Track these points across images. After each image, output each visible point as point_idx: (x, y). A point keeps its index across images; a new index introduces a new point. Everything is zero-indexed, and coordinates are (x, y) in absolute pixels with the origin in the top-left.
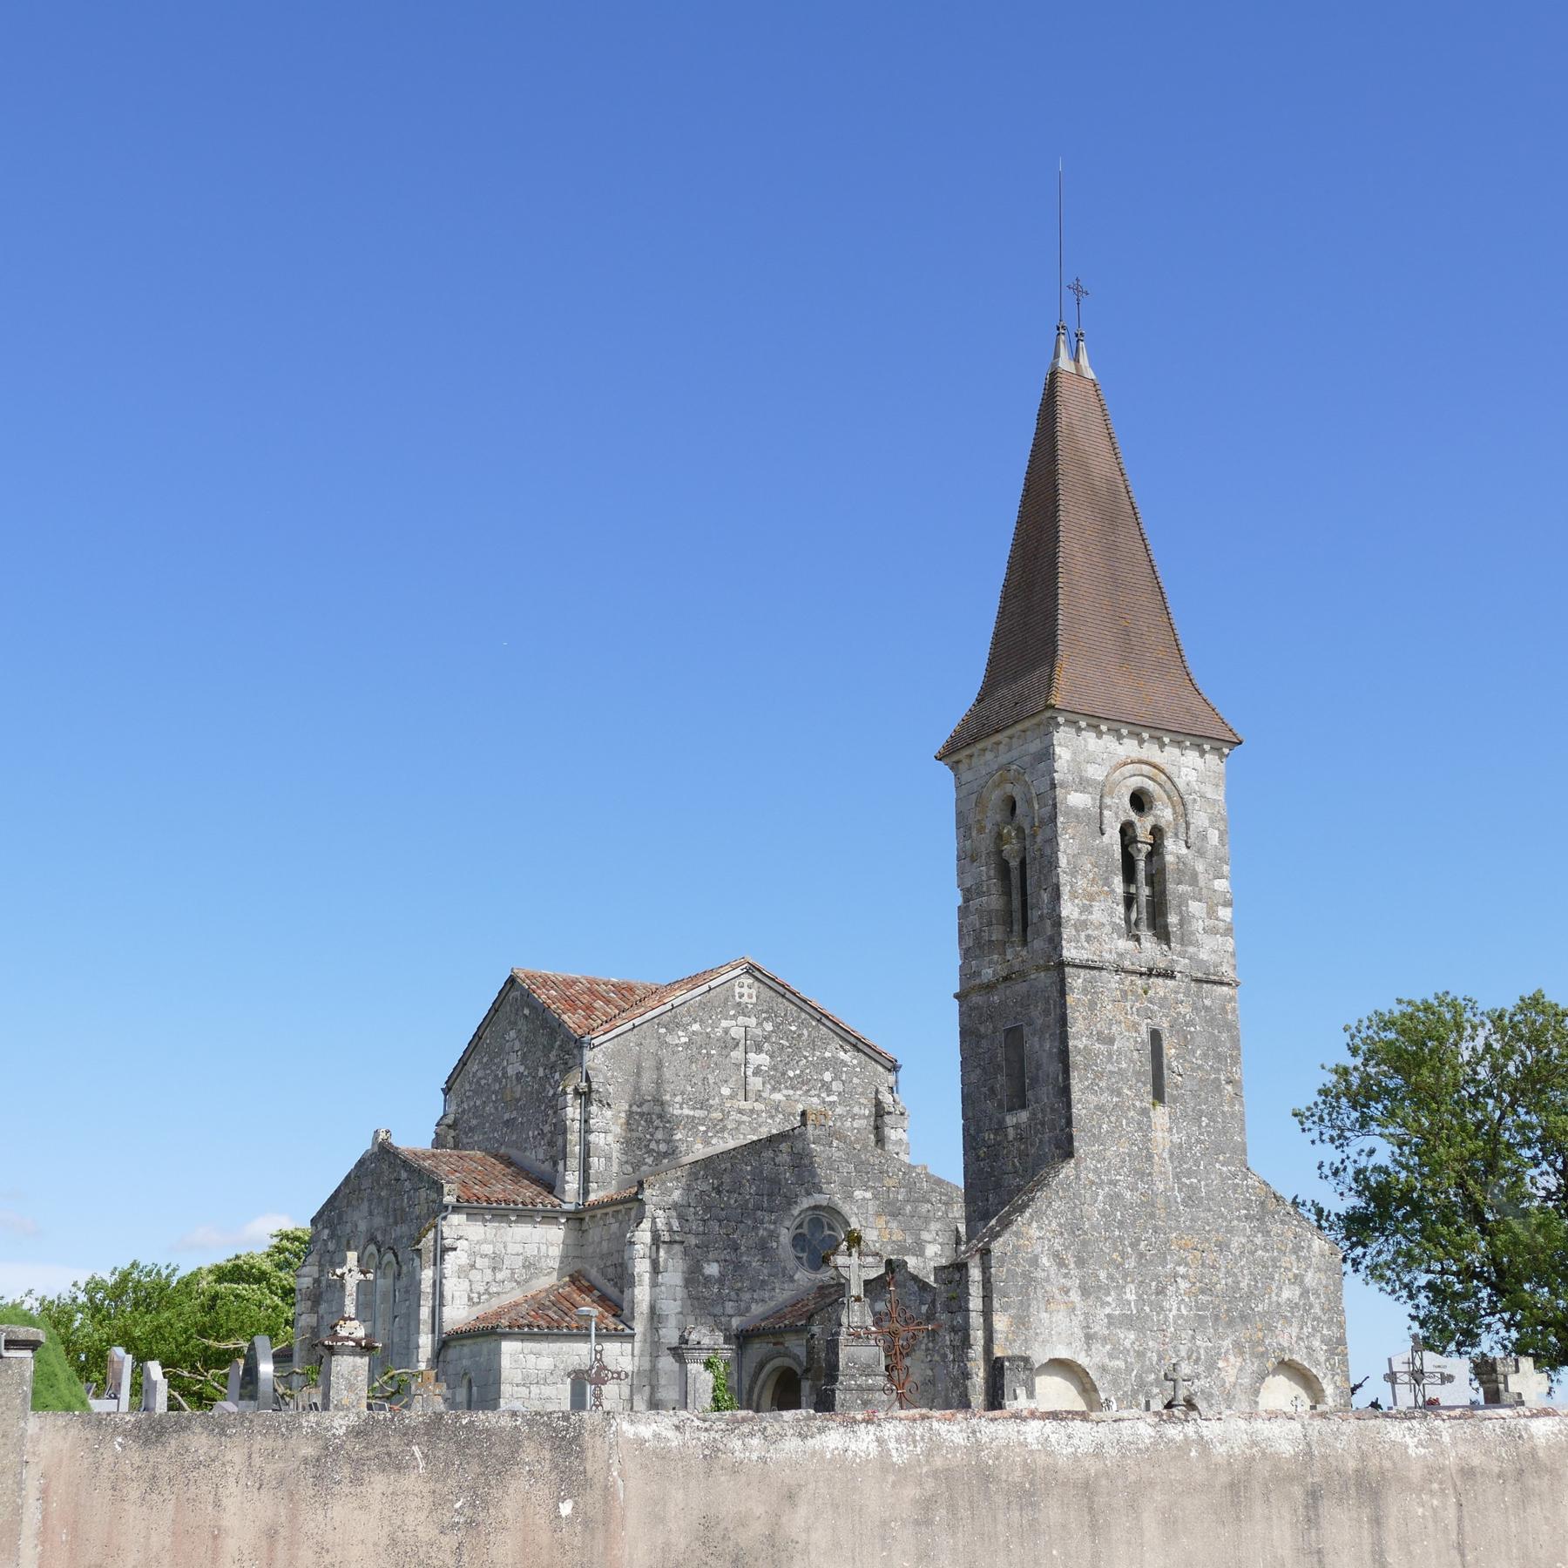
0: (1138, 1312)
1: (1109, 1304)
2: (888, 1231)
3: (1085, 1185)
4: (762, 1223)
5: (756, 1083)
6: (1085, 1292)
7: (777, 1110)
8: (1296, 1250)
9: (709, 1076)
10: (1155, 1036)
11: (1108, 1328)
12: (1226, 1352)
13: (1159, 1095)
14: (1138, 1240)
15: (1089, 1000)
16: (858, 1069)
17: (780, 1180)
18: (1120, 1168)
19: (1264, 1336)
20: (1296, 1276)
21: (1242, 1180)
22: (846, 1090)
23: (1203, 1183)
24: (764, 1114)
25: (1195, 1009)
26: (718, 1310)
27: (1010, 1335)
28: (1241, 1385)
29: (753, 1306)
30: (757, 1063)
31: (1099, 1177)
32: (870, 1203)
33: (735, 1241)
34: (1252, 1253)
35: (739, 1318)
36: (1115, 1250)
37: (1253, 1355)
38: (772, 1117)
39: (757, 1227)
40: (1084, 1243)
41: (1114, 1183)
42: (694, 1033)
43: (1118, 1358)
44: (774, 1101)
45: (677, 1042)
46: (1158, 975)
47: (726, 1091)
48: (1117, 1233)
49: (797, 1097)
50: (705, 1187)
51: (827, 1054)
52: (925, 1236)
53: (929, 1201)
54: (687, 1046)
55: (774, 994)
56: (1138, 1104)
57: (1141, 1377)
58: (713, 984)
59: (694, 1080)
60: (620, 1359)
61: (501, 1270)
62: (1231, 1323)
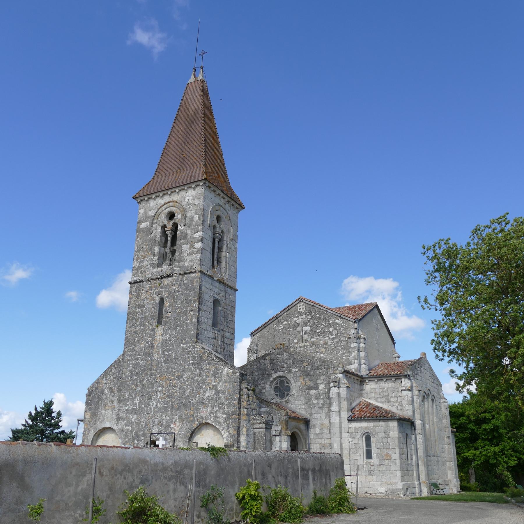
0: (139, 407)
1: (128, 405)
3: (126, 361)
4: (260, 384)
5: (305, 337)
6: (119, 401)
7: (313, 344)
8: (214, 375)
10: (162, 300)
11: (126, 414)
12: (176, 421)
13: (159, 323)
14: (143, 380)
15: (137, 294)
16: (343, 325)
18: (140, 353)
19: (194, 413)
20: (213, 386)
21: (192, 349)
22: (338, 333)
23: (174, 353)
24: (308, 347)
25: (180, 286)
27: (90, 420)
28: (180, 434)
30: (306, 330)
31: (131, 357)
32: (298, 372)
34: (193, 378)
36: (133, 384)
37: (188, 421)
38: (311, 347)
40: (122, 383)
41: (137, 359)
42: (285, 324)
43: (129, 426)
44: (312, 341)
46: (165, 277)
47: (295, 341)
48: (135, 378)
49: (320, 339)
51: (331, 322)
52: (319, 382)
56: (151, 327)
57: (137, 433)
62: (178, 409)
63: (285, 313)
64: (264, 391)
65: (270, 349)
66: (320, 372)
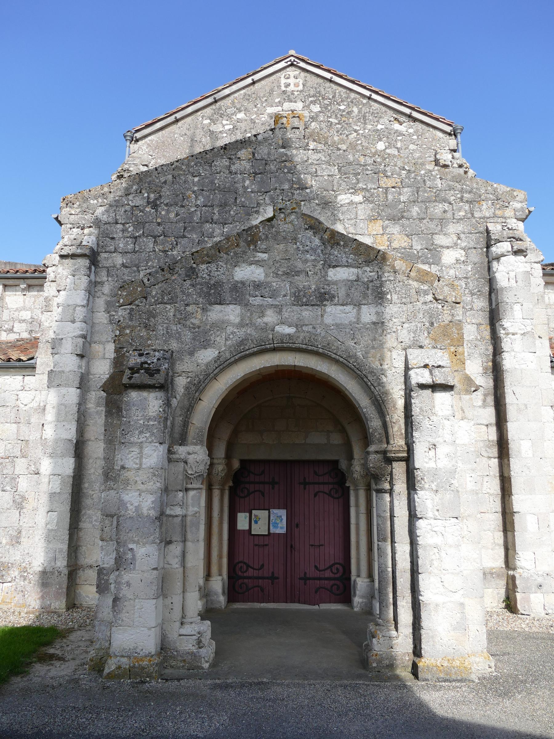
2: (385, 237)
16: (415, 137)
17: (237, 188)
32: (360, 207)
39: (204, 241)
42: (239, 121)
45: (221, 129)
50: (138, 201)
51: (380, 127)
53: (445, 200)
55: (321, 81)
63: (242, 92)
66: (445, 212)
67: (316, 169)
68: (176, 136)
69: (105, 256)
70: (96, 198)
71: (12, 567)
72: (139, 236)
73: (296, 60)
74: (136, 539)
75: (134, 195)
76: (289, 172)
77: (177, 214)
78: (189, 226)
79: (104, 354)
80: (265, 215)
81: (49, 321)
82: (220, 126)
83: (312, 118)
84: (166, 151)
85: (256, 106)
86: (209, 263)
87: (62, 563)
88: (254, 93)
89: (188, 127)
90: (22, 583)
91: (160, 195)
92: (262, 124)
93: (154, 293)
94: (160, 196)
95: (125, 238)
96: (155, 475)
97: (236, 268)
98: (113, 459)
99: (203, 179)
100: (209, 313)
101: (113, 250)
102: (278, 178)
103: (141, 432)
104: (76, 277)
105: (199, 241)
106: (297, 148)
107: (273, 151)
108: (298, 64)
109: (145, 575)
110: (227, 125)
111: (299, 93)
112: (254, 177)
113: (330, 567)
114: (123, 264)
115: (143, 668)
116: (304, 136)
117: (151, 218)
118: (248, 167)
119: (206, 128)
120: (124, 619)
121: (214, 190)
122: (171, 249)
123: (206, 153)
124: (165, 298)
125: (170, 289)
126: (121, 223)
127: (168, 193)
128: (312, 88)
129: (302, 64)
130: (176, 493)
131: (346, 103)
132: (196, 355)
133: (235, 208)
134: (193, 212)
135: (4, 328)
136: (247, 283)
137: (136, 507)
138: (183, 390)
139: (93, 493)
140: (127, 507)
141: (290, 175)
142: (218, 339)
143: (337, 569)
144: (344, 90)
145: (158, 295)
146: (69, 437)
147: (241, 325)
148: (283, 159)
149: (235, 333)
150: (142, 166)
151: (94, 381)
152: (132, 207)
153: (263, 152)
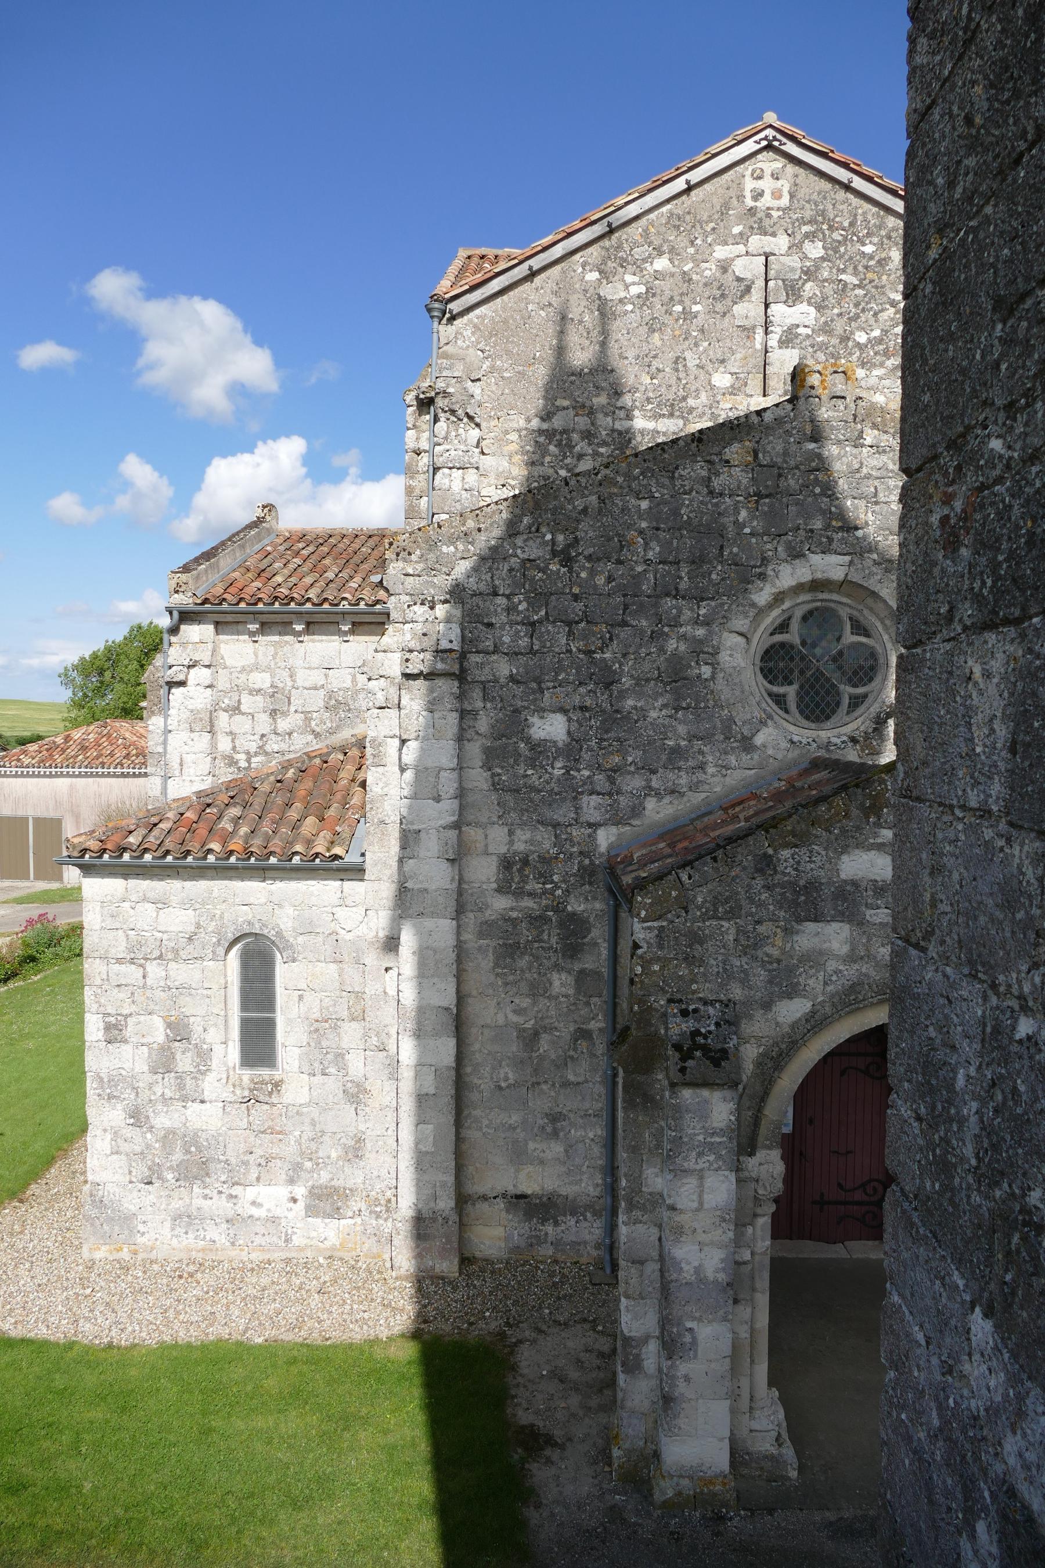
4: (676, 623)
9: (688, 355)
17: (724, 527)
26: (563, 813)
29: (651, 804)
30: (789, 321)
33: (605, 666)
35: (614, 830)
39: (663, 633)
42: (658, 275)
45: (623, 294)
47: (722, 380)
49: (873, 381)
50: (534, 551)
54: (644, 300)
55: (827, 186)
58: (695, 176)
59: (656, 364)
60: (340, 913)
61: (285, 714)
63: (664, 209)
64: (706, 671)
65: (560, 409)
67: (876, 488)
68: (530, 307)
69: (478, 660)
70: (452, 541)
71: (353, 1195)
72: (540, 622)
73: (779, 136)
74: (697, 1315)
75: (525, 537)
76: (823, 494)
77: (609, 577)
78: (634, 604)
79: (486, 846)
80: (777, 581)
81: (381, 785)
82: (620, 286)
83: (807, 272)
84: (512, 342)
85: (692, 243)
86: (796, 846)
87: (446, 1203)
88: (689, 213)
89: (555, 288)
90: (374, 1222)
91: (576, 538)
92: (706, 285)
93: (700, 899)
94: (576, 540)
95: (512, 624)
96: (725, 1221)
97: (843, 857)
98: (640, 1176)
99: (658, 504)
100: (795, 938)
101: (491, 648)
102: (802, 505)
103: (700, 1155)
104: (437, 715)
105: (653, 632)
106: (839, 442)
107: (794, 448)
108: (782, 147)
109: (713, 1365)
110: (634, 284)
111: (781, 213)
112: (757, 502)
113: (863, 1185)
114: (511, 676)
115: (715, 1495)
116: (855, 416)
117: (560, 585)
118: (745, 481)
119: (591, 290)
120: (682, 1426)
121: (679, 529)
122: (601, 649)
123: (663, 449)
124: (720, 910)
125: (727, 894)
126: (503, 595)
127: (591, 534)
128: (808, 202)
129: (791, 148)
130: (743, 1229)
131: (875, 240)
132: (774, 1009)
133: (719, 568)
134: (639, 573)
135: (223, 705)
136: (864, 884)
137: (695, 1267)
138: (751, 1067)
139: (481, 1081)
140: (681, 1268)
141: (825, 499)
142: (811, 982)
143: (875, 1189)
144: (875, 210)
145: (708, 905)
146: (445, 1004)
147: (852, 958)
148: (814, 464)
149: (841, 971)
150: (470, 383)
151: (472, 895)
152: (524, 561)
153: (774, 448)
